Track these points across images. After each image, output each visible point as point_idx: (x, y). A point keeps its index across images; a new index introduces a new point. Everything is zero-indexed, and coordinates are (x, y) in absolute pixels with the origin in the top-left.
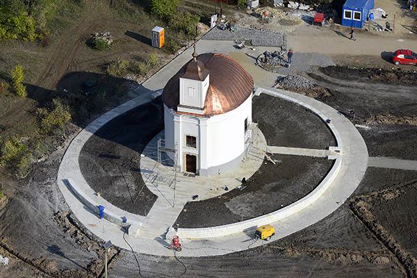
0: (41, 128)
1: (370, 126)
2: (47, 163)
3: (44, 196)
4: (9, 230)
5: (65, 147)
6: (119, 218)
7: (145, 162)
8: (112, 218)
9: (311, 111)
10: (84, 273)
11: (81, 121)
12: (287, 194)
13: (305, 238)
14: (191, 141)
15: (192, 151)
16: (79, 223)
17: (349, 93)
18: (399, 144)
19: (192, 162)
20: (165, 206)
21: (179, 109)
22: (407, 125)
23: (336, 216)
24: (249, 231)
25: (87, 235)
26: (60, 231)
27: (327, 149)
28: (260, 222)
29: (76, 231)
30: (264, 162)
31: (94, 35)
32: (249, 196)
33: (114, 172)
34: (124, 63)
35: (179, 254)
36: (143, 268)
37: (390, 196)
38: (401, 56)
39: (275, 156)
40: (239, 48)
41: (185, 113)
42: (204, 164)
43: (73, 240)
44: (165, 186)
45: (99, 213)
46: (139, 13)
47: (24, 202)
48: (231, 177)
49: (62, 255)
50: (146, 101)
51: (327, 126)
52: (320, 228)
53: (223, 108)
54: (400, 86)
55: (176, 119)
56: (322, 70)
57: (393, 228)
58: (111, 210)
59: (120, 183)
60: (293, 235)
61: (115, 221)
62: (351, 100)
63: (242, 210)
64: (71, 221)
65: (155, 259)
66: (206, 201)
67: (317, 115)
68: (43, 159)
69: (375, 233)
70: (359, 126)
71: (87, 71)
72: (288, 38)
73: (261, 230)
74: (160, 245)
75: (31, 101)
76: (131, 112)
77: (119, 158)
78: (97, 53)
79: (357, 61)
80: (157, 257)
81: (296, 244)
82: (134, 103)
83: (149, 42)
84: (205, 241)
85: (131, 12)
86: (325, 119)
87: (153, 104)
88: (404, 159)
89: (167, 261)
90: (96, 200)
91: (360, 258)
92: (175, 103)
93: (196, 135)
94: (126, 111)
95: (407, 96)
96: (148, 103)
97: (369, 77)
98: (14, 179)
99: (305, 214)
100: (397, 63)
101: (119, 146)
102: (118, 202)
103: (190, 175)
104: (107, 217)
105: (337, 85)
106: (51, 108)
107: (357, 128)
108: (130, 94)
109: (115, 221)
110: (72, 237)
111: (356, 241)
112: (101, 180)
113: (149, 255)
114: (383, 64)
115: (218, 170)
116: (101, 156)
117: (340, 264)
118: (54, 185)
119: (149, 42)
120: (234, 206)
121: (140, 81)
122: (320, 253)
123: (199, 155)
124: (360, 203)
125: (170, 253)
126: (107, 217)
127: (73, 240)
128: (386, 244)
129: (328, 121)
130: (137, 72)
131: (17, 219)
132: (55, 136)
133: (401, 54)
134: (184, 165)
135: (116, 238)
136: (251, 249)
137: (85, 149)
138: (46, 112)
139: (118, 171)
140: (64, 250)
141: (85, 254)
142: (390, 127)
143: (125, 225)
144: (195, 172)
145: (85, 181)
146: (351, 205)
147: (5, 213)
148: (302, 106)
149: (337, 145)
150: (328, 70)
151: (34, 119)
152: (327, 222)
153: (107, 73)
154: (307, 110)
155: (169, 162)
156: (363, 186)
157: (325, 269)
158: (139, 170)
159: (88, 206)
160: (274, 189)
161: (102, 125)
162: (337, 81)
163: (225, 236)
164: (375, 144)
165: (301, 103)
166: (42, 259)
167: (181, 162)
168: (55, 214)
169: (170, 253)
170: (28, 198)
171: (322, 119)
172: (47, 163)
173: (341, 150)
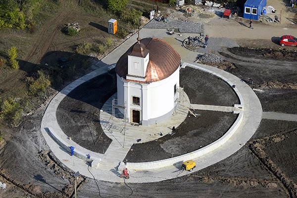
0: (29, 91)
1: (264, 89)
2: (33, 116)
3: (32, 140)
4: (6, 164)
5: (47, 105)
6: (85, 155)
7: (103, 115)
8: (80, 156)
9: (221, 79)
10: (60, 194)
11: (58, 86)
12: (204, 138)
13: (217, 170)
14: (136, 100)
15: (137, 108)
16: (56, 159)
17: (248, 66)
18: (284, 103)
19: (137, 116)
20: (118, 147)
21: (128, 78)
22: (290, 89)
23: (239, 154)
24: (177, 165)
25: (62, 167)
26: (43, 165)
27: (233, 106)
28: (185, 158)
29: (54, 165)
30: (188, 116)
31: (67, 25)
32: (178, 140)
33: (81, 123)
34: (88, 45)
35: (128, 181)
36: (102, 191)
37: (278, 140)
38: (286, 40)
39: (196, 111)
40: (170, 34)
41: (132, 80)
42: (145, 117)
43: (52, 171)
44: (117, 133)
45: (71, 152)
46: (99, 9)
47: (17, 144)
48: (165, 126)
49: (44, 181)
50: (104, 72)
51: (233, 89)
52: (228, 162)
53: (159, 77)
54: (285, 62)
55: (125, 84)
56: (230, 50)
57: (280, 162)
58: (79, 149)
59: (85, 130)
60: (209, 168)
61: (82, 157)
62: (250, 71)
63: (172, 149)
64: (51, 157)
65: (111, 185)
66: (147, 143)
67: (226, 82)
68: (31, 113)
69: (267, 166)
70: (256, 90)
71: (62, 51)
72: (205, 27)
73: (186, 164)
74: (114, 174)
75: (22, 72)
76: (93, 80)
77: (85, 112)
78: (69, 38)
79: (254, 43)
80: (112, 183)
81: (211, 174)
82: (96, 73)
83: (106, 30)
84: (146, 172)
85: (94, 9)
86: (231, 85)
87: (109, 74)
88: (288, 113)
89: (119, 186)
90: (69, 143)
91: (256, 184)
92: (125, 73)
93: (140, 96)
94: (89, 79)
95: (290, 68)
96: (105, 73)
97: (263, 55)
98: (10, 127)
99: (217, 152)
100: (283, 45)
101: (85, 104)
102: (84, 144)
103: (135, 125)
104: (76, 155)
105: (240, 60)
106: (37, 77)
107: (254, 91)
108: (93, 67)
109: (82, 157)
110: (51, 169)
111: (253, 172)
112: (72, 128)
113: (106, 182)
114: (273, 46)
115: (155, 121)
116: (72, 111)
117: (242, 188)
118: (38, 132)
119: (106, 30)
120: (167, 146)
121: (100, 57)
122: (228, 180)
123: (142, 110)
124: (257, 145)
125: (121, 180)
126: (76, 155)
127: (52, 171)
128: (275, 174)
129: (234, 86)
130: (98, 51)
131: (12, 156)
132: (39, 97)
133: (286, 38)
134: (131, 117)
135: (83, 170)
136: (179, 178)
137: (61, 106)
138: (33, 80)
139: (84, 122)
140: (45, 178)
141: (60, 181)
142: (277, 90)
143: (89, 160)
144: (139, 123)
145: (60, 129)
146: (250, 146)
147: (4, 152)
148: (215, 76)
149: (240, 104)
150: (233, 50)
151: (24, 85)
152: (233, 158)
153: (76, 52)
154: (219, 78)
155: (120, 116)
156: (259, 133)
157: (232, 192)
158: (99, 121)
159: (63, 147)
160: (195, 135)
161: (73, 89)
162: (240, 58)
163: (160, 168)
164: (267, 102)
165: (214, 74)
166: (30, 185)
167: (129, 115)
168: (39, 153)
169: (121, 180)
170: (20, 141)
171: (229, 85)
172: (33, 116)
173: (243, 107)
